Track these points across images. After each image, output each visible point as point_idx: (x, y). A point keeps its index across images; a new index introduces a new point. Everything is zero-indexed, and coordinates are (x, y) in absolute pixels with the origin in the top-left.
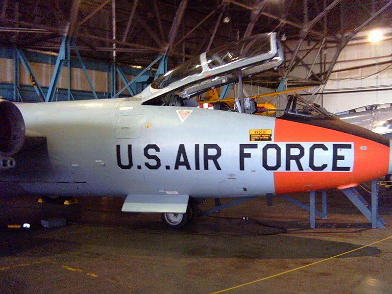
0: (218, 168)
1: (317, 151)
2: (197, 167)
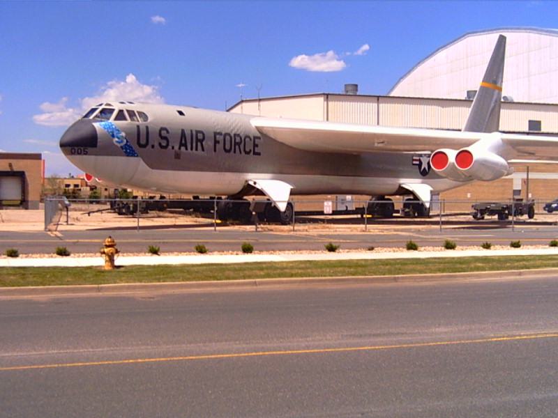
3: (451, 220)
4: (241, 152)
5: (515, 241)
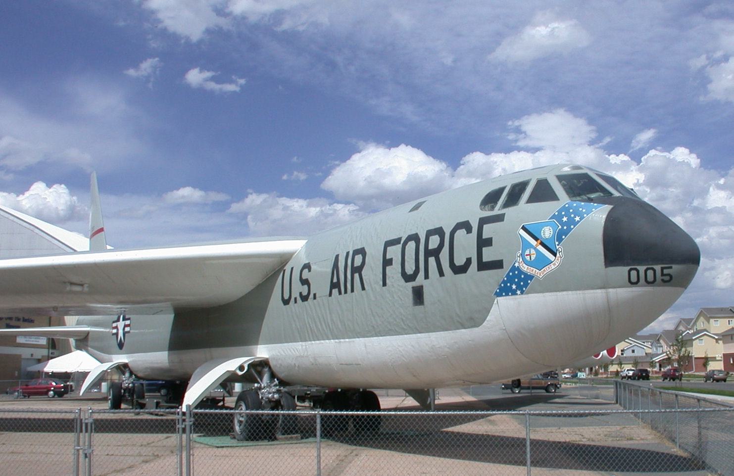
0: (363, 288)
1: (461, 233)
2: (346, 292)
3: (343, 281)
4: (441, 274)
5: (317, 296)
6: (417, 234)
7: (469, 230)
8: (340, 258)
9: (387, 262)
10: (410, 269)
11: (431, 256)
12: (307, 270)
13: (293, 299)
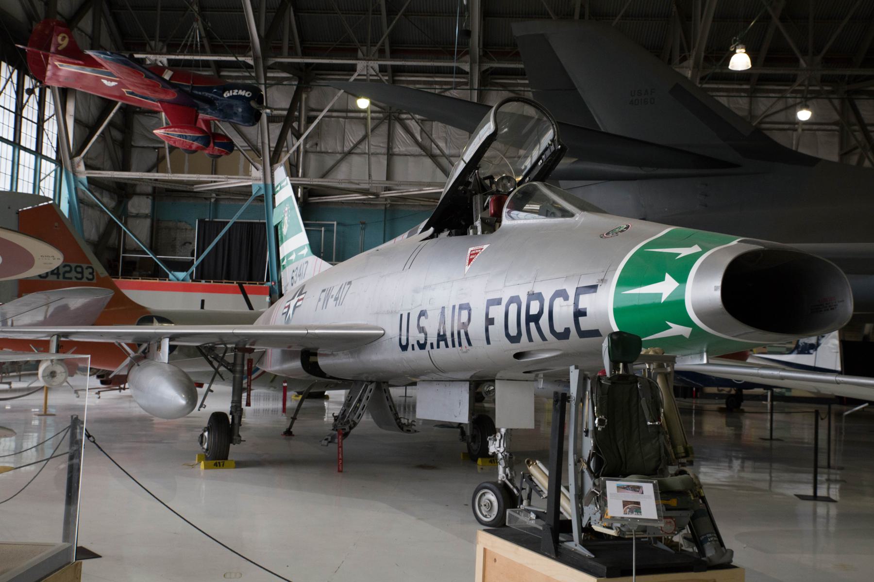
2: (454, 346)
6: (468, 304)
7: (566, 298)
8: (446, 310)
9: (490, 321)
10: (513, 332)
11: (532, 322)
12: (422, 318)
13: (410, 347)
